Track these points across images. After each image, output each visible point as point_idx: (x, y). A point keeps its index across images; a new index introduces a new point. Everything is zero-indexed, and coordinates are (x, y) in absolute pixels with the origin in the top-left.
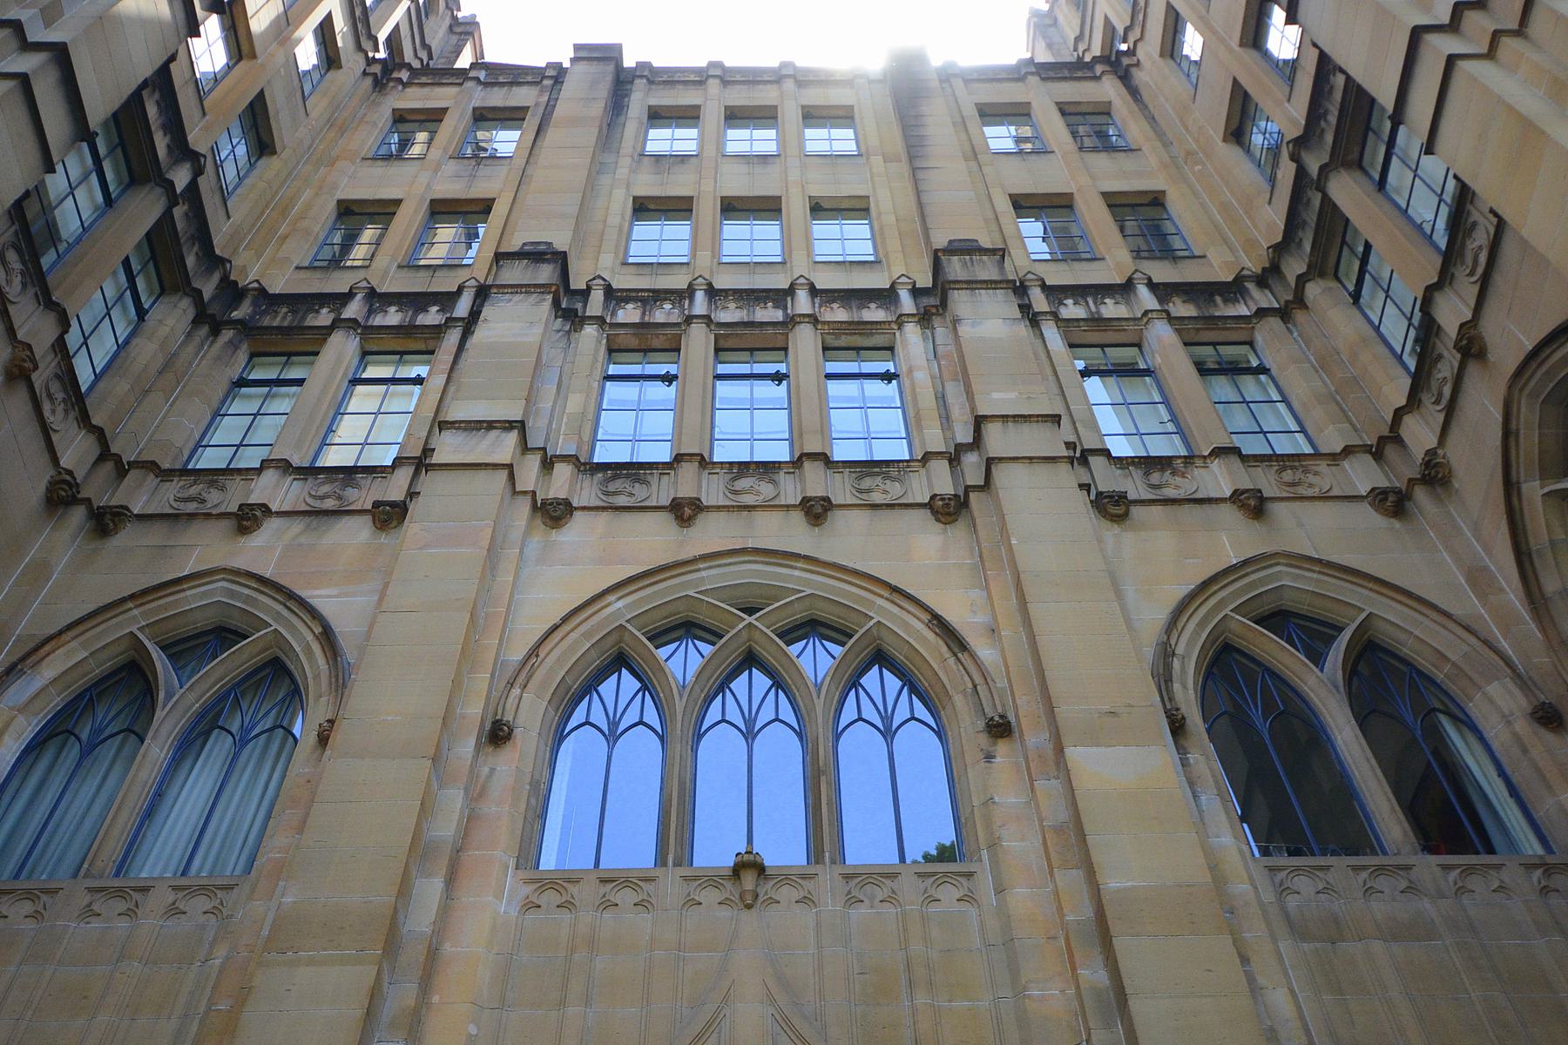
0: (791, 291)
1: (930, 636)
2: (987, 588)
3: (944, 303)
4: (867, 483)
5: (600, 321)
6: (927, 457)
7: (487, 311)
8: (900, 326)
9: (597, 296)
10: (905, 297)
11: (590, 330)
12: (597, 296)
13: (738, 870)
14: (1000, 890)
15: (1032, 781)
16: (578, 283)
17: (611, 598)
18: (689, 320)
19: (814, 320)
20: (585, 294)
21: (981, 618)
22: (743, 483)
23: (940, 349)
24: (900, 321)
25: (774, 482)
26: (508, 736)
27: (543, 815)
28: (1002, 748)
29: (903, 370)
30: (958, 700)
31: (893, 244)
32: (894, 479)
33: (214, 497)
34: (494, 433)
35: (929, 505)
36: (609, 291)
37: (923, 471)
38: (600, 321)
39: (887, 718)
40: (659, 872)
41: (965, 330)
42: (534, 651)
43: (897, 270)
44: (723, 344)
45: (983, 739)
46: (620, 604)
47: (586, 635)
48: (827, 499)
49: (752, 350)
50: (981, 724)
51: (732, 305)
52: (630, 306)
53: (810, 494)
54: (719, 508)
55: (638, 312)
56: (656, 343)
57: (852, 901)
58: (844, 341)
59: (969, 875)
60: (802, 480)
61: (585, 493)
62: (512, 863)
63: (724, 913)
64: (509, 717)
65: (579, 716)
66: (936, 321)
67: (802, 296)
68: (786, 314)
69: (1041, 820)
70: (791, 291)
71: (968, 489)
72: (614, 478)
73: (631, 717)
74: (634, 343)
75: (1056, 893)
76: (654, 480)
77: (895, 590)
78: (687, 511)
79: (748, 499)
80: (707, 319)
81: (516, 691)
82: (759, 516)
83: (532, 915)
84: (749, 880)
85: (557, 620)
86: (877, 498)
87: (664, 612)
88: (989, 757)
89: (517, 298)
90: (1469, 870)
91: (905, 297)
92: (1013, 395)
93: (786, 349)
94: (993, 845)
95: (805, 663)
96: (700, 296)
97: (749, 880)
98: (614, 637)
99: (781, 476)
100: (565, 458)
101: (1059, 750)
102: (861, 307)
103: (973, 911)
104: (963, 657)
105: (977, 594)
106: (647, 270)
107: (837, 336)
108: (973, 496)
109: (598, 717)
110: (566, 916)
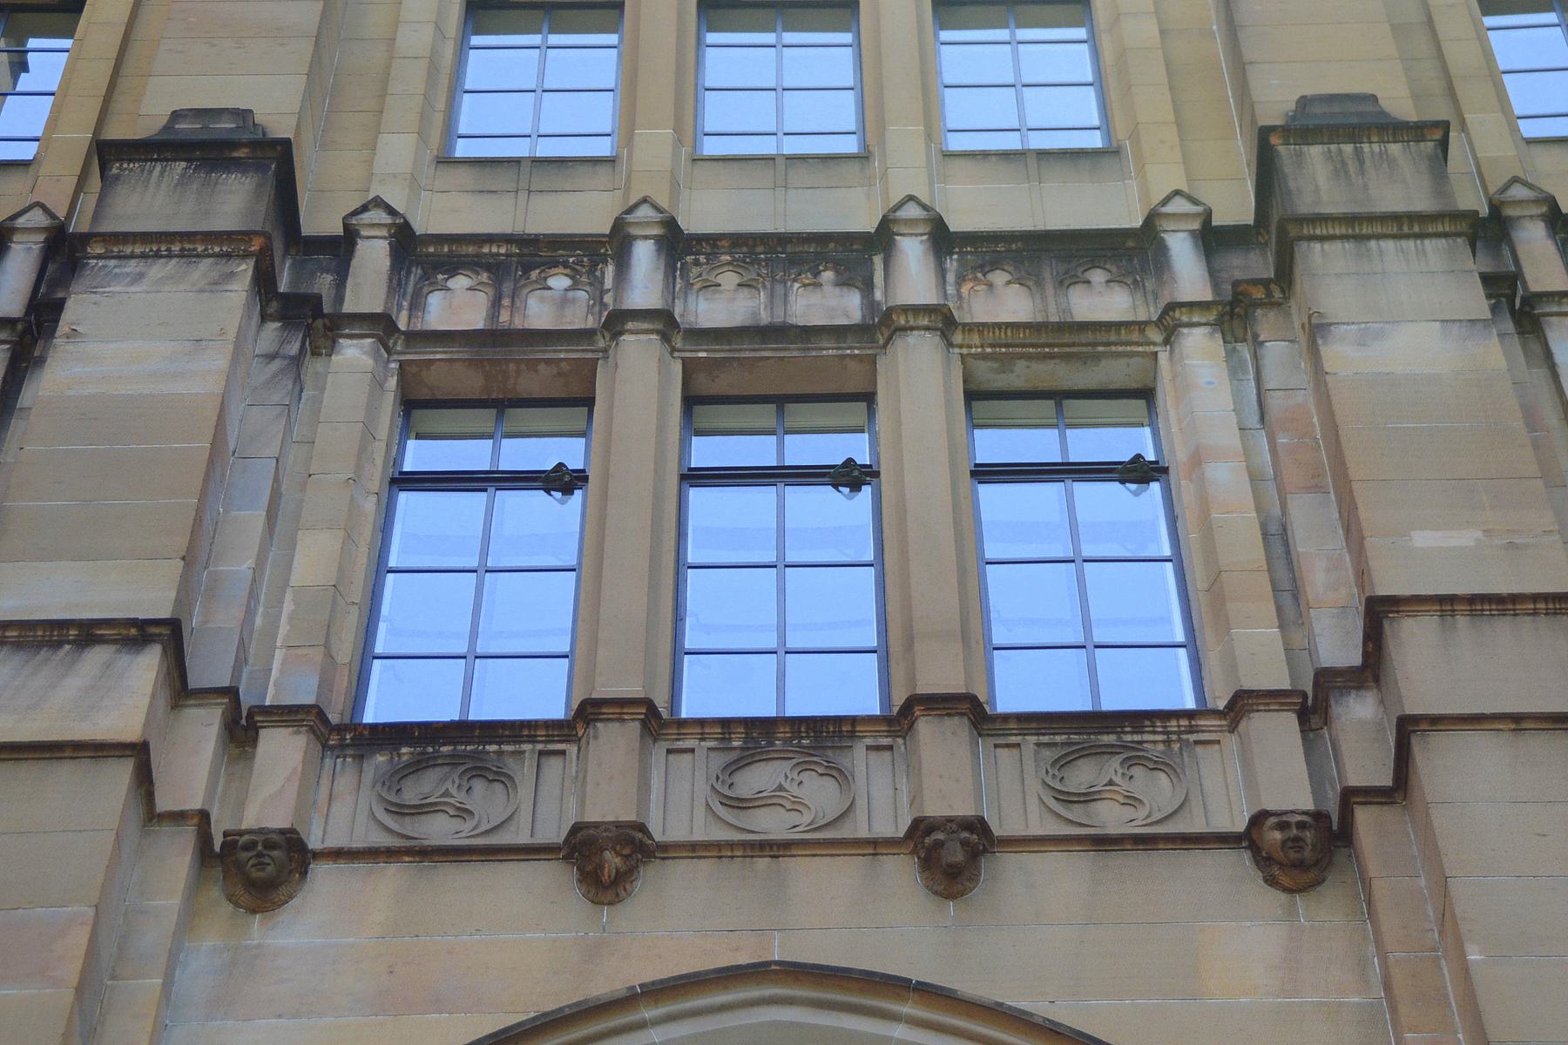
0: (882, 239)
3: (1285, 274)
4: (1083, 775)
5: (381, 326)
6: (1242, 704)
7: (79, 309)
8: (1170, 334)
9: (373, 255)
10: (1182, 251)
11: (354, 353)
12: (373, 255)
16: (319, 219)
18: (617, 322)
19: (943, 321)
20: (341, 248)
22: (760, 778)
23: (1276, 402)
24: (1171, 320)
25: (840, 775)
29: (1178, 458)
31: (1153, 102)
32: (1157, 766)
33: (486, 802)
34: (97, 656)
35: (1248, 839)
36: (405, 241)
37: (1231, 742)
38: (381, 326)
41: (1340, 354)
43: (1165, 177)
44: (705, 385)
48: (978, 826)
49: (781, 401)
51: (729, 279)
52: (460, 282)
53: (935, 809)
54: (695, 849)
55: (482, 299)
56: (530, 385)
58: (1020, 375)
60: (913, 769)
61: (341, 810)
66: (1266, 323)
67: (912, 251)
68: (870, 304)
70: (882, 239)
71: (1350, 796)
72: (419, 766)
74: (471, 383)
76: (524, 771)
78: (612, 861)
79: (771, 824)
80: (664, 322)
82: (804, 872)
86: (1111, 817)
89: (158, 269)
91: (1182, 251)
92: (1465, 538)
93: (869, 398)
96: (644, 255)
99: (859, 758)
100: (288, 715)
102: (1067, 280)
106: (504, 179)
107: (1005, 362)
108: (1364, 817)
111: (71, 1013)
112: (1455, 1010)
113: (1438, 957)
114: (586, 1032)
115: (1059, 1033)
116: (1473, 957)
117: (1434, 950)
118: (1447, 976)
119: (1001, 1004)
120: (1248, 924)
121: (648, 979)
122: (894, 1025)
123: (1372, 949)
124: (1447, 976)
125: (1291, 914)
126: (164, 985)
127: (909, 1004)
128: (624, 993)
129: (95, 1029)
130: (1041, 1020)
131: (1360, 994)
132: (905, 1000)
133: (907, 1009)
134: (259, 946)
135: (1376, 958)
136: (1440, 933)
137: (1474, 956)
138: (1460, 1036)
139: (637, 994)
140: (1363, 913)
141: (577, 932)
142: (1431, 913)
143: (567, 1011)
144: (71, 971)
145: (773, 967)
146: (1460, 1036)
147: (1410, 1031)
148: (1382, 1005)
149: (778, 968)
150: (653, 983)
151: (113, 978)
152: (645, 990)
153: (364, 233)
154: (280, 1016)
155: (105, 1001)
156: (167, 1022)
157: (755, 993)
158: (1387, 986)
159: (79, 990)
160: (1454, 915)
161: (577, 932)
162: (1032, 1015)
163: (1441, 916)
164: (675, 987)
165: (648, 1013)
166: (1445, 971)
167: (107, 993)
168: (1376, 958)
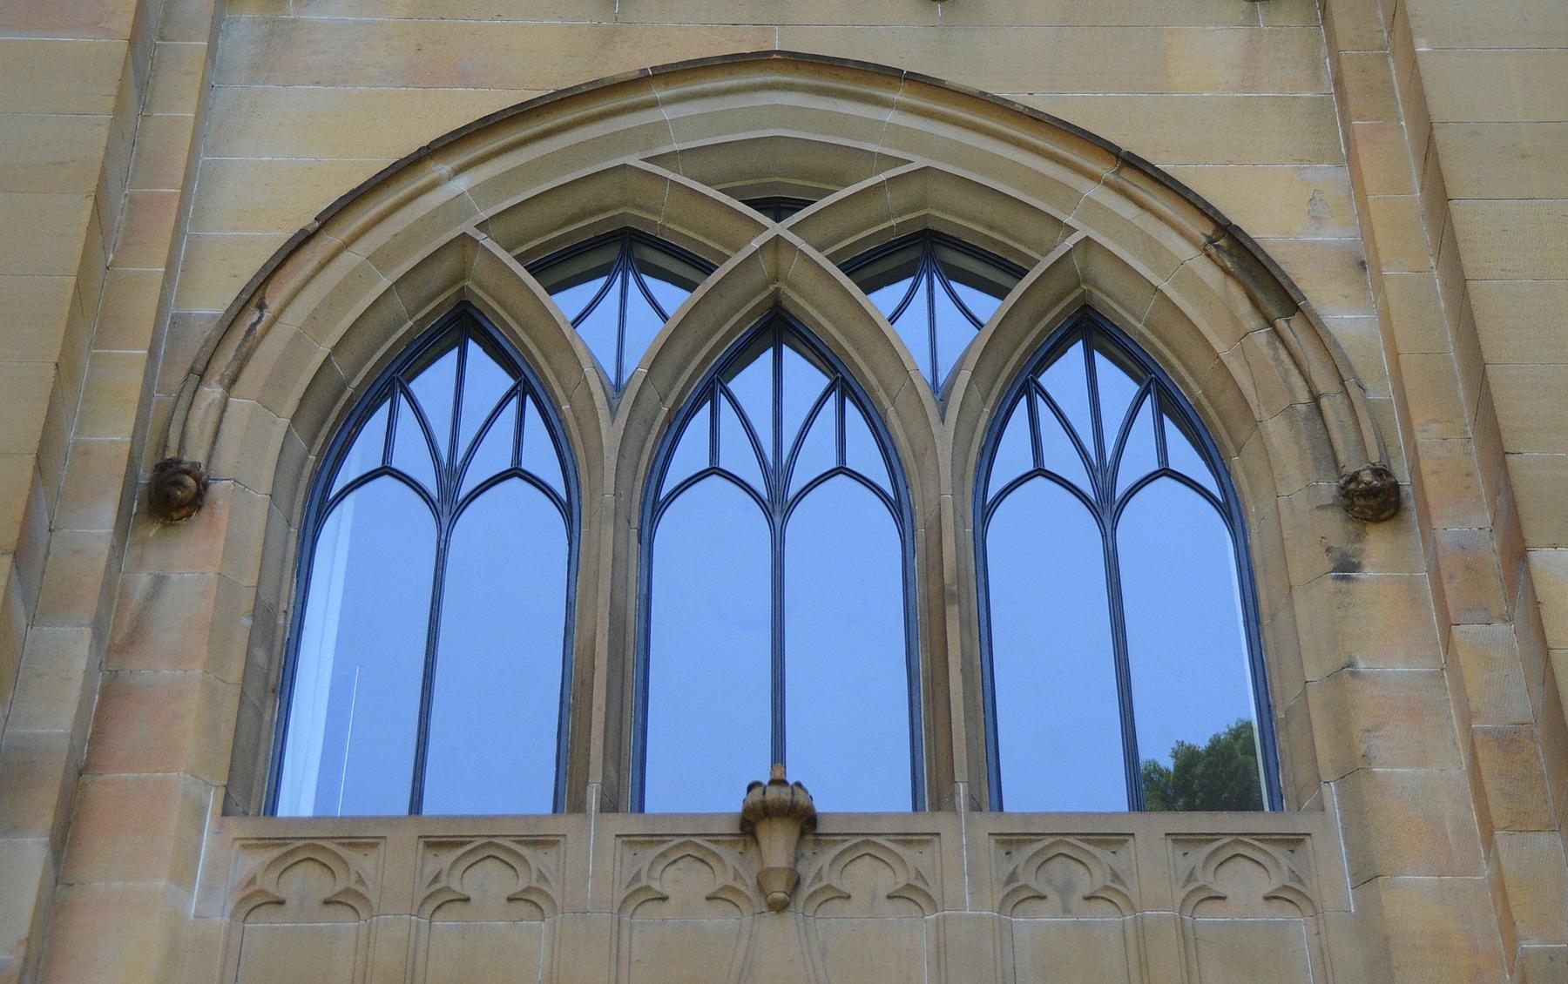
1: (1210, 274)
2: (1352, 159)
13: (751, 823)
14: (1365, 877)
15: (1447, 625)
17: (440, 168)
21: (1337, 233)
26: (198, 501)
27: (283, 687)
28: (1377, 545)
30: (1276, 430)
39: (1103, 469)
40: (924, 823)
42: (254, 295)
45: (1334, 526)
46: (461, 184)
47: (381, 259)
50: (1328, 489)
57: (1019, 896)
59: (1294, 841)
62: (213, 801)
63: (720, 920)
64: (196, 453)
65: (363, 454)
69: (1467, 717)
73: (493, 456)
75: (1500, 888)
77: (1129, 162)
81: (212, 392)
83: (262, 925)
84: (777, 844)
85: (307, 220)
87: (566, 206)
88: (1346, 567)
90: (1232, 849)
94: (1354, 771)
95: (910, 334)
97: (777, 844)
98: (448, 265)
101: (1517, 554)
103: (1299, 925)
104: (1292, 329)
105: (1328, 177)
109: (412, 456)
110: (345, 925)
111: (125, 62)
112: (1399, 100)
113: (1386, 56)
114: (600, 108)
115: (1038, 120)
116: (1421, 49)
117: (1382, 48)
118: (1394, 73)
119: (985, 94)
120: (1213, 28)
121: (659, 63)
122: (886, 111)
123: (1324, 50)
124: (1394, 73)
125: (1251, 19)
126: (166, 273)
127: (899, 93)
128: (637, 75)
129: (148, 83)
130: (1022, 108)
131: (1312, 91)
132: (895, 88)
133: (898, 96)
134: (294, 21)
135: (1327, 60)
136: (1389, 33)
137: (1422, 48)
138: (1403, 123)
139: (649, 76)
140: (1317, 19)
141: (592, 21)
142: (1381, 17)
143: (584, 89)
144: (124, 23)
145: (774, 56)
146: (1403, 123)
147: (1358, 119)
148: (1331, 100)
149: (779, 57)
150: (663, 67)
151: (162, 39)
152: (656, 73)
153: (171, 454)
154: (318, 83)
155: (155, 58)
156: (213, 83)
157: (759, 78)
158: (1338, 82)
159: (132, 41)
160: (1405, 13)
161: (592, 21)
162: (1013, 103)
163: (1392, 17)
164: (685, 71)
165: (659, 93)
166: (1392, 67)
167: (156, 51)
168: (1327, 60)
